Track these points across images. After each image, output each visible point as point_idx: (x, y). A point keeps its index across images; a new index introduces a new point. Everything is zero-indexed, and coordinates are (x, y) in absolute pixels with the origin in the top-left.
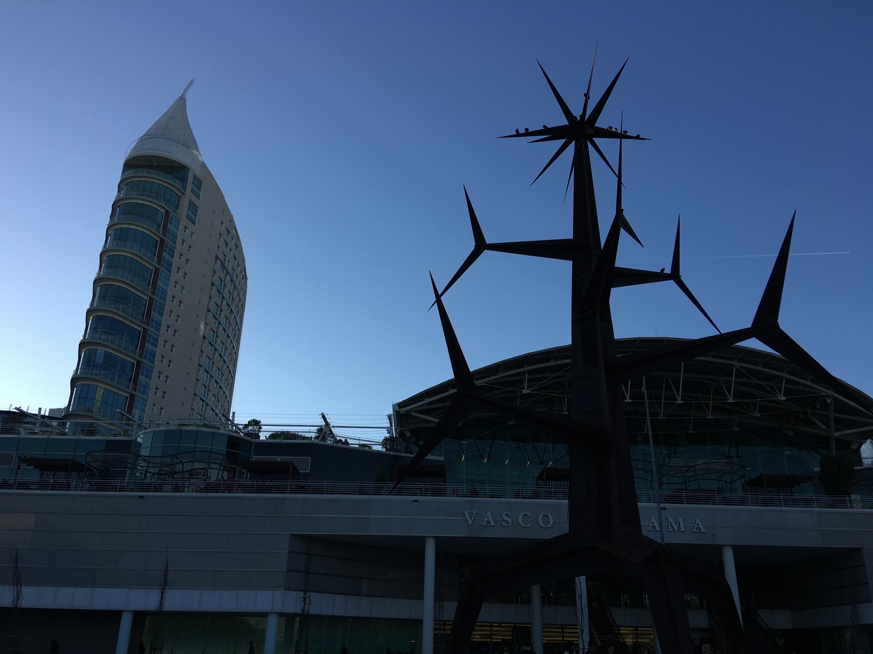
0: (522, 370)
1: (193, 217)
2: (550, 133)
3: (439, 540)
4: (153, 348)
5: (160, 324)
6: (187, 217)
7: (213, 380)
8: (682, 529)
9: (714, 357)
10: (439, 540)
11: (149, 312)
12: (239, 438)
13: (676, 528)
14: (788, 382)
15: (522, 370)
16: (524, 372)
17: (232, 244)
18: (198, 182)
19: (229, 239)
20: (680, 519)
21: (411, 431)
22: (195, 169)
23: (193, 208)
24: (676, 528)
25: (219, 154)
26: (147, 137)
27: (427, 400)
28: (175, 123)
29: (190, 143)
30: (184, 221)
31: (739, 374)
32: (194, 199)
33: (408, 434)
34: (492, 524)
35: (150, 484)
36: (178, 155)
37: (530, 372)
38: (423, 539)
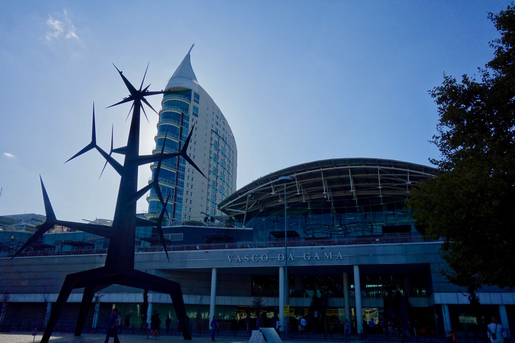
0: (269, 183)
1: (196, 113)
2: (126, 100)
3: (218, 270)
4: (182, 180)
5: (184, 168)
6: (193, 114)
7: (218, 192)
8: (331, 258)
9: (351, 165)
10: (218, 270)
11: (178, 164)
12: (65, 234)
13: (328, 258)
14: (410, 173)
15: (269, 183)
16: (270, 185)
17: (220, 123)
18: (197, 96)
19: (218, 121)
20: (331, 253)
21: (235, 216)
22: (194, 90)
23: (196, 109)
24: (328, 258)
25: (205, 80)
26: (172, 79)
27: (230, 202)
28: (185, 69)
29: (192, 77)
30: (191, 116)
31: (381, 172)
32: (196, 104)
33: (234, 218)
34: (319, 259)
35: (101, 250)
36: (185, 84)
37: (274, 184)
38: (211, 270)
